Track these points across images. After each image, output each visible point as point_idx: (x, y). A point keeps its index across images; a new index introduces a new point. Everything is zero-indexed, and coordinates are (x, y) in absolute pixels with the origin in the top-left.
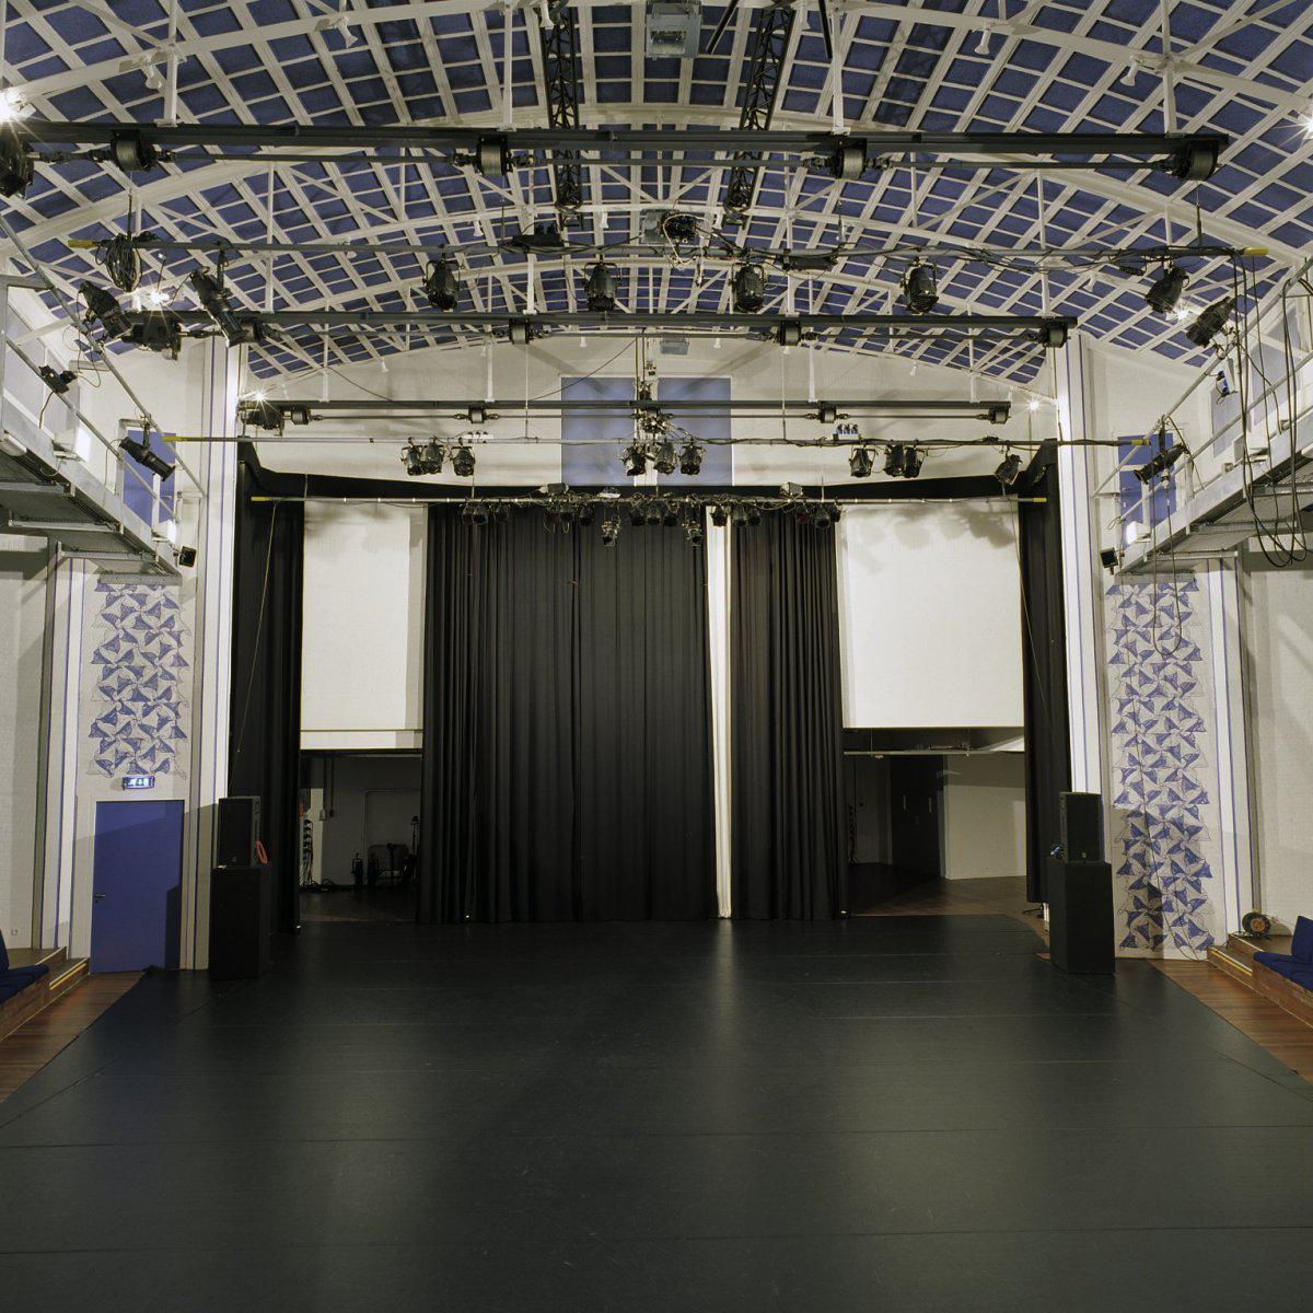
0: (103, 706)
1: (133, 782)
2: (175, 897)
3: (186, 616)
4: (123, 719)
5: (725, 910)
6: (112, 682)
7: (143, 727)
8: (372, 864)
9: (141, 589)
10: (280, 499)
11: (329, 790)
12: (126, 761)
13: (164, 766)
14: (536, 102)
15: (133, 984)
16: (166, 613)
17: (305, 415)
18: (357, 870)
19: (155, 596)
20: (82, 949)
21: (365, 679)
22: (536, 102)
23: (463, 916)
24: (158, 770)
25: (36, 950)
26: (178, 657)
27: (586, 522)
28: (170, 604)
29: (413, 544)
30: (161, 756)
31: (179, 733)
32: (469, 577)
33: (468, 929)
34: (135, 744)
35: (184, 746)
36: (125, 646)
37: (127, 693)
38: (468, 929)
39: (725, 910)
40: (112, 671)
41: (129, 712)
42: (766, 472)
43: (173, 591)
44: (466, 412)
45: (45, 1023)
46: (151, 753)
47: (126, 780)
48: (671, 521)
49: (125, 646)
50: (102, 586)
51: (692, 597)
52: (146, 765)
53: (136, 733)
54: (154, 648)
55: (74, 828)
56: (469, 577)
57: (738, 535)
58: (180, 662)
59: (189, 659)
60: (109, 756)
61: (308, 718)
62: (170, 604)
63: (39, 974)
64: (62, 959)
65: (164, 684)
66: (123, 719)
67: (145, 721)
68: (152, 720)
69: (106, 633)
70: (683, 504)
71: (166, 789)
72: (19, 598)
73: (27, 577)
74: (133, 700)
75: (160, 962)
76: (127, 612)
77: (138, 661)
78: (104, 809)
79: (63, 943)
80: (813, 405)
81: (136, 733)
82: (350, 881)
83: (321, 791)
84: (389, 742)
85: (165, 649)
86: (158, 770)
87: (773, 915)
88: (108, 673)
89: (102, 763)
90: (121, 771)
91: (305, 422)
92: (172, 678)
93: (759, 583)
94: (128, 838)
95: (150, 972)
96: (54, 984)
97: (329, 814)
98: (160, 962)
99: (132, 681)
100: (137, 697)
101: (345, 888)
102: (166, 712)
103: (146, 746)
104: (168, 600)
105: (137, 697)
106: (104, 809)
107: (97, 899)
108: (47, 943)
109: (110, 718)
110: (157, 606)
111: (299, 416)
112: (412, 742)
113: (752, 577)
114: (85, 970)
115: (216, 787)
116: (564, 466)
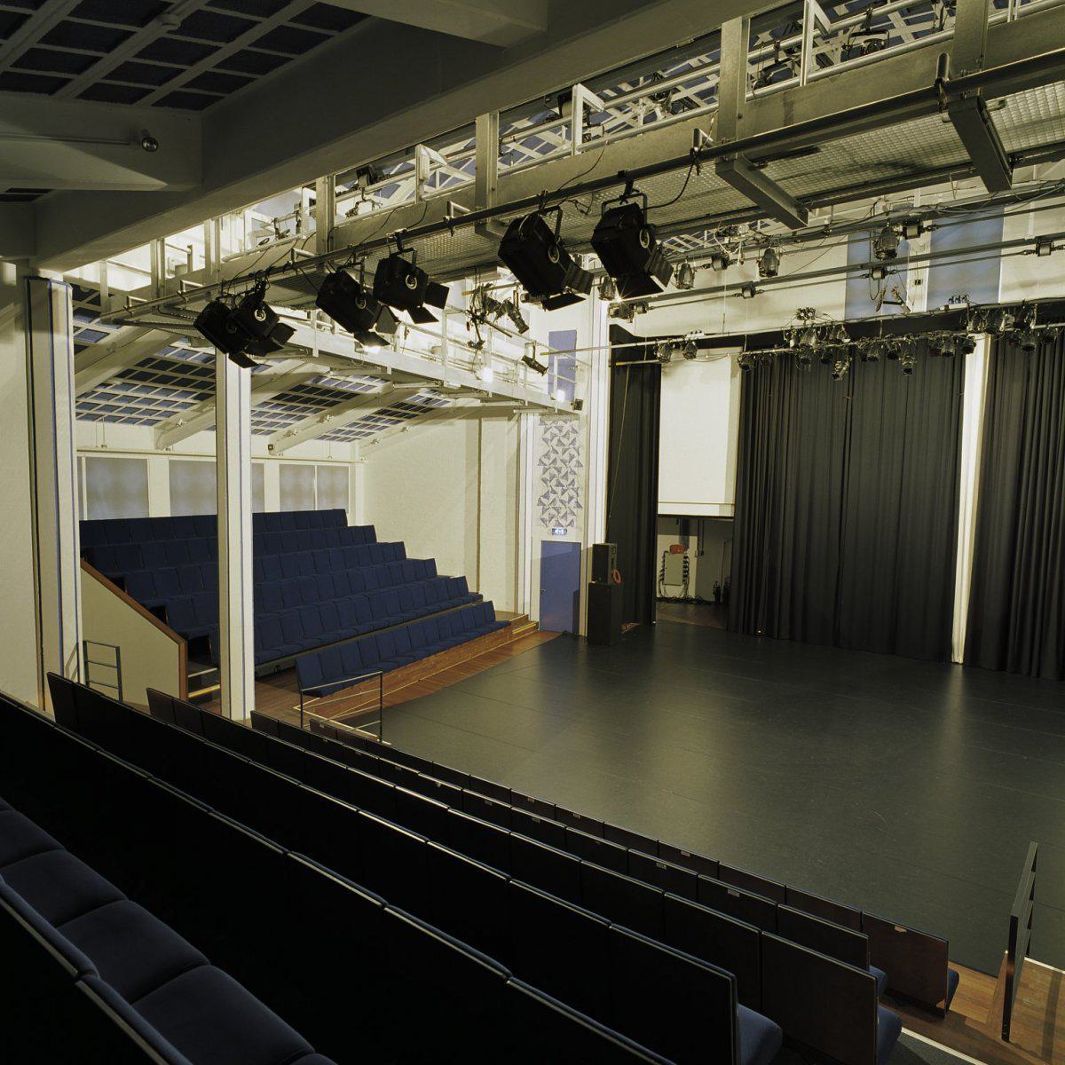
0: (543, 489)
1: (556, 531)
2: (577, 595)
3: (581, 439)
4: (552, 496)
5: (958, 657)
6: (547, 476)
7: (561, 501)
8: (725, 589)
9: (560, 423)
10: (631, 363)
11: (701, 538)
12: (553, 520)
13: (571, 523)
14: (263, 465)
15: (552, 638)
16: (572, 436)
17: (644, 308)
18: (717, 592)
19: (567, 427)
20: (535, 617)
21: (699, 468)
22: (263, 465)
23: (756, 630)
24: (569, 525)
25: (515, 614)
26: (578, 462)
27: (825, 361)
28: (575, 431)
29: (733, 375)
30: (570, 518)
31: (579, 506)
32: (770, 398)
33: (759, 640)
34: (558, 510)
35: (581, 512)
36: (553, 456)
37: (554, 482)
38: (759, 640)
39: (958, 657)
40: (547, 470)
41: (555, 493)
42: (1034, 287)
43: (575, 423)
44: (740, 291)
45: (511, 650)
46: (565, 516)
47: (554, 530)
48: (893, 356)
49: (553, 456)
50: (542, 422)
51: (947, 406)
52: (562, 522)
53: (558, 504)
54: (566, 457)
55: (532, 557)
56: (770, 398)
57: (998, 347)
58: (579, 464)
59: (583, 463)
60: (546, 516)
61: (663, 494)
62: (575, 431)
63: (507, 625)
64: (526, 619)
65: (571, 477)
66: (552, 496)
67: (562, 498)
68: (565, 497)
69: (544, 449)
70: (902, 342)
71: (572, 536)
72: (506, 431)
73: (509, 420)
74: (557, 486)
75: (570, 630)
76: (554, 436)
77: (559, 464)
78: (545, 544)
79: (527, 612)
80: (1030, 242)
81: (558, 504)
82: (712, 598)
83: (696, 538)
84: (714, 511)
85: (572, 457)
86: (569, 525)
87: (1002, 665)
88: (545, 471)
89: (543, 520)
90: (552, 525)
91: (644, 312)
92: (575, 473)
93: (1015, 391)
94: (556, 560)
95: (565, 634)
96: (515, 632)
97: (701, 553)
98: (570, 630)
99: (558, 478)
100: (559, 484)
101: (708, 603)
102: (573, 493)
103: (563, 512)
104: (573, 429)
105: (559, 484)
106: (545, 544)
107: (542, 592)
108: (520, 611)
109: (546, 496)
110: (568, 432)
111: (640, 309)
112: (728, 512)
113: (1007, 385)
114: (536, 628)
115: (598, 536)
116: (847, 304)
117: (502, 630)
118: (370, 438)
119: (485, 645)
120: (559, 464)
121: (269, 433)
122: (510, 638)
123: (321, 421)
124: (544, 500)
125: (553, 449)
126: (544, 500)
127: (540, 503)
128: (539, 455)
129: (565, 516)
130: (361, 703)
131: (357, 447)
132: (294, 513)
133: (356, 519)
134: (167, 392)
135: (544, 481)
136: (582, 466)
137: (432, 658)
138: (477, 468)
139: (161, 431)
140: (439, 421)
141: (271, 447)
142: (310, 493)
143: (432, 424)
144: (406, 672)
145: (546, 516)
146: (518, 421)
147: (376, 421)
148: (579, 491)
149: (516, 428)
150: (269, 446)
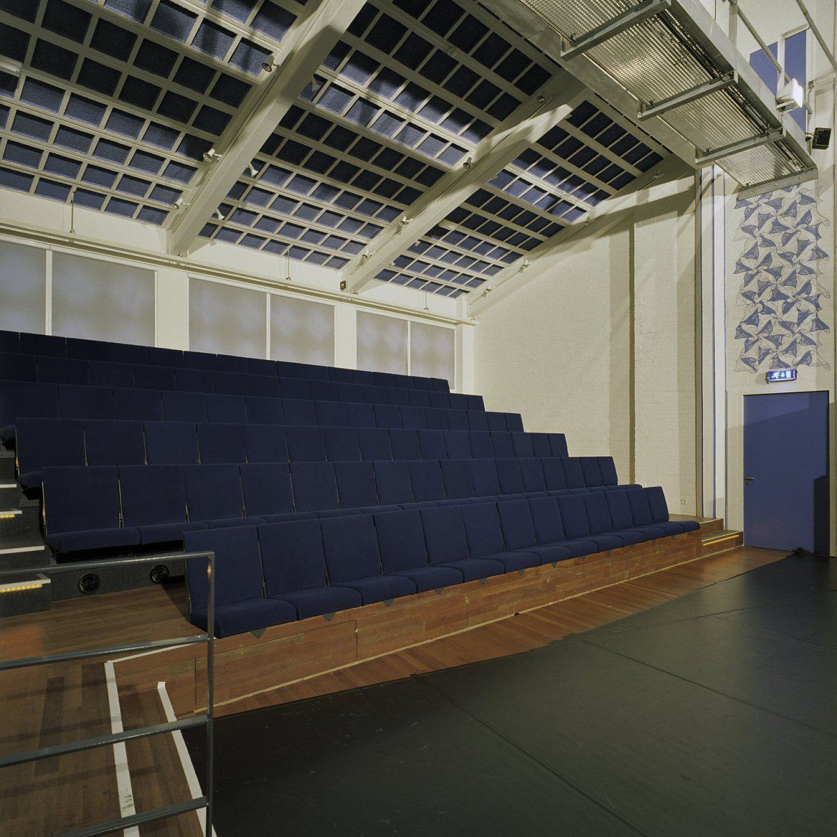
1: (776, 375)
7: (783, 324)
12: (768, 358)
15: (781, 558)
24: (801, 362)
28: (806, 199)
30: (802, 350)
34: (776, 341)
36: (763, 252)
40: (752, 277)
43: (809, 186)
46: (792, 348)
47: (770, 374)
60: (753, 353)
62: (806, 199)
64: (718, 526)
65: (802, 280)
67: (785, 318)
68: (792, 316)
72: (675, 233)
74: (773, 299)
75: (809, 546)
78: (750, 400)
79: (720, 515)
81: (777, 330)
86: (801, 362)
88: (749, 279)
90: (764, 368)
96: (707, 541)
98: (809, 546)
100: (777, 296)
105: (777, 296)
106: (750, 400)
107: (747, 481)
108: (708, 513)
109: (752, 320)
110: (793, 206)
117: (684, 536)
118: (482, 287)
119: (652, 559)
120: (777, 262)
121: (340, 262)
122: (699, 553)
123: (398, 231)
124: (748, 328)
125: (765, 240)
126: (748, 328)
127: (740, 332)
128: (734, 257)
129: (792, 348)
130: (357, 657)
131: (465, 304)
132: (375, 373)
133: (463, 385)
134: (130, 123)
135: (748, 295)
136: (825, 255)
137: (547, 570)
138: (628, 300)
139: (171, 231)
140: (572, 243)
141: (343, 285)
142: (401, 354)
143: (560, 251)
144: (485, 593)
145: (753, 353)
146: (697, 213)
147: (482, 250)
148: (821, 301)
149: (693, 220)
150: (341, 283)
